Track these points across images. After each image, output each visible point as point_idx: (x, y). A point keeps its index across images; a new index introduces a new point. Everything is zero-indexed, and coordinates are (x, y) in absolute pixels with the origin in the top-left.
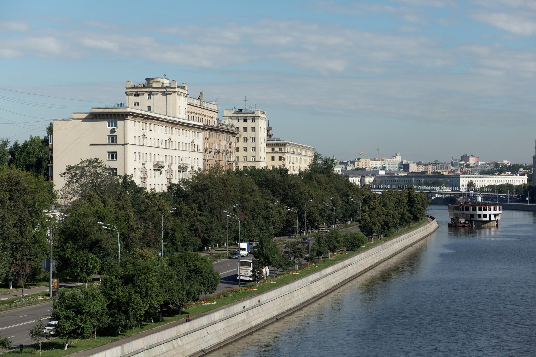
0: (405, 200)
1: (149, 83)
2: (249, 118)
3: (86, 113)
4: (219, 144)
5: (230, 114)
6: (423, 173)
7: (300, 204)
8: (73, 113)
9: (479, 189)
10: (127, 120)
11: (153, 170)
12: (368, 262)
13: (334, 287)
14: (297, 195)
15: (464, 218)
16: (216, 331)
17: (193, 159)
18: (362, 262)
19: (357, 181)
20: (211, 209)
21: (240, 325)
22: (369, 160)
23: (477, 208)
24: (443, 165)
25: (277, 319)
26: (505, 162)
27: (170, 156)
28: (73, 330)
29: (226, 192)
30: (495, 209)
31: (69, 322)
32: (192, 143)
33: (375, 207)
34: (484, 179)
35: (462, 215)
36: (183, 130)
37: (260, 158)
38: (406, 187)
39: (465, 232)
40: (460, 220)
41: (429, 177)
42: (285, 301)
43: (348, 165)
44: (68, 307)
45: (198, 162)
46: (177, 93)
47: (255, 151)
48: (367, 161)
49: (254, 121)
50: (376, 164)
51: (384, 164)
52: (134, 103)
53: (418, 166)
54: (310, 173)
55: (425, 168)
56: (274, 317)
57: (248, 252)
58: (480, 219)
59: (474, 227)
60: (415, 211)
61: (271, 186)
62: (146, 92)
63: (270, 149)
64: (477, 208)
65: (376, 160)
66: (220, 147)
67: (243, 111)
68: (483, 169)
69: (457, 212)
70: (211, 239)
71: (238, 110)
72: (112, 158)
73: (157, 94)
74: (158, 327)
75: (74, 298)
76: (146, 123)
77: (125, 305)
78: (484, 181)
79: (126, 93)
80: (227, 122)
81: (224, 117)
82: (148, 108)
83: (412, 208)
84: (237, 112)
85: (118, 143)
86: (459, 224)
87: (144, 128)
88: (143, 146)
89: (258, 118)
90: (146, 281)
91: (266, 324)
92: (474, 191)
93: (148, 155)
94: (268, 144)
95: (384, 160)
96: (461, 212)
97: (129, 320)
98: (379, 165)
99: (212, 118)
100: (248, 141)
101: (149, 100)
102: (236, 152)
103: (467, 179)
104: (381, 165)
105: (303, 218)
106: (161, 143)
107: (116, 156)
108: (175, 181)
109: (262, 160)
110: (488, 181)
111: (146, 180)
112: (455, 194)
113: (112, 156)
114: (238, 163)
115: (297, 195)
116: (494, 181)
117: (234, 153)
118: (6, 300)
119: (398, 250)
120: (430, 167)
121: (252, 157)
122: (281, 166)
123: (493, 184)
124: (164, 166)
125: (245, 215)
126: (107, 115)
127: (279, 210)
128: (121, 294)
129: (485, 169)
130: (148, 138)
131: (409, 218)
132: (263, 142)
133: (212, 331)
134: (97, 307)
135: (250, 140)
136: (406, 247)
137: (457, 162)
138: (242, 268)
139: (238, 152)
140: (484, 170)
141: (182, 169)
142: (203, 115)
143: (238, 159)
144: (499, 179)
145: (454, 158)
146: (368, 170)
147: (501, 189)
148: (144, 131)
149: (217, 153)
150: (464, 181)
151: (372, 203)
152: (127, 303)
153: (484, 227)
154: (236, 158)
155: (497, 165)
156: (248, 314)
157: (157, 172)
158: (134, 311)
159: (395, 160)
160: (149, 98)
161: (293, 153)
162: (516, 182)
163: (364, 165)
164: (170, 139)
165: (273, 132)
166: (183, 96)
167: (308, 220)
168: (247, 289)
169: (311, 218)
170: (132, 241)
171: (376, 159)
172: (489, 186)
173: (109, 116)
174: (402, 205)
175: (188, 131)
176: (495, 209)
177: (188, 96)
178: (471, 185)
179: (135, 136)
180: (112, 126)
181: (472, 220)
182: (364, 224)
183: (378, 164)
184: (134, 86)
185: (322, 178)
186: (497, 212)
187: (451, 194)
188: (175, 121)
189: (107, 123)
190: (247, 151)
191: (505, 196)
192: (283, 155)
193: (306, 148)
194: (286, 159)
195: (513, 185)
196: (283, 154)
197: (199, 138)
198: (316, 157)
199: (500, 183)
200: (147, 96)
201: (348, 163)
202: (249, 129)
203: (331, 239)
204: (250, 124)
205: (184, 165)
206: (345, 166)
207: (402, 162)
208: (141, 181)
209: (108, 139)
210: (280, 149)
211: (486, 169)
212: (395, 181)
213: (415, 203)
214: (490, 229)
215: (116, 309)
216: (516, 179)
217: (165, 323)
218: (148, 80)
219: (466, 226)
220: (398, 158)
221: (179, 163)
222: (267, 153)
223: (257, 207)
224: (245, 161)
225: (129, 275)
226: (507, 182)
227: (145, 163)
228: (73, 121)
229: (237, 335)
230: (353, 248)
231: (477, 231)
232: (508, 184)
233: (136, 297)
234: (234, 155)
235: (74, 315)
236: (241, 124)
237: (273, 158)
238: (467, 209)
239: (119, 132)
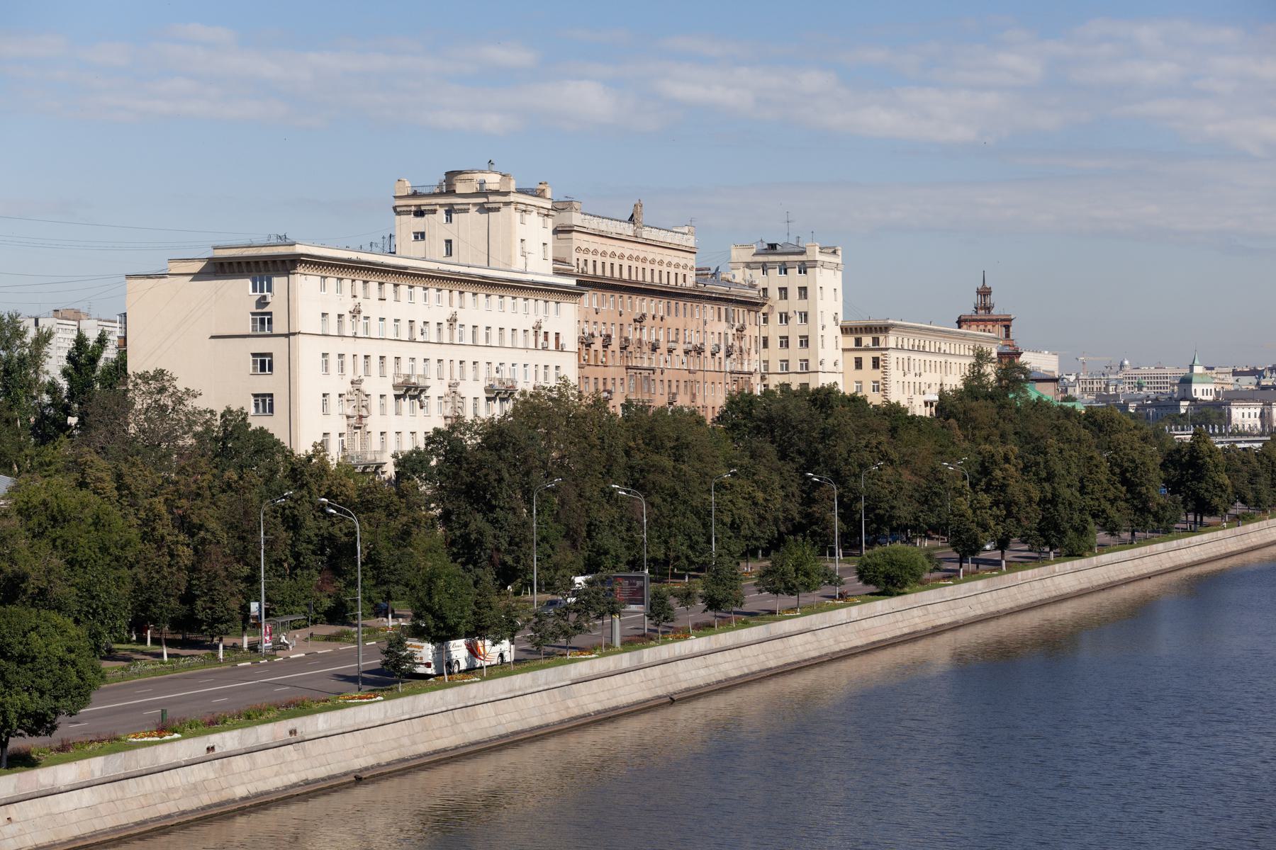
2: (792, 265)
3: (200, 260)
4: (701, 329)
5: (747, 256)
8: (171, 260)
10: (294, 274)
16: (51, 814)
19: (1252, 415)
43: (1264, 378)
46: (513, 207)
47: (807, 345)
52: (414, 233)
60: (1207, 490)
62: (441, 205)
63: (850, 342)
67: (778, 247)
71: (766, 247)
72: (263, 369)
73: (466, 211)
79: (395, 208)
81: (731, 265)
82: (447, 245)
83: (1199, 482)
85: (274, 332)
88: (354, 337)
89: (814, 264)
94: (846, 329)
100: (789, 322)
101: (449, 225)
105: (857, 512)
107: (271, 363)
111: (364, 422)
113: (263, 363)
114: (767, 376)
118: (84, 708)
121: (800, 360)
122: (878, 382)
124: (428, 387)
126: (248, 263)
138: (414, 644)
139: (766, 350)
143: (766, 368)
148: (357, 300)
154: (762, 365)
160: (449, 220)
165: (993, 299)
166: (534, 213)
169: (882, 512)
173: (253, 264)
180: (262, 291)
182: (958, 527)
189: (250, 284)
192: (883, 355)
196: (884, 352)
200: (445, 216)
202: (793, 293)
204: (794, 279)
206: (1256, 381)
208: (348, 425)
209: (253, 323)
210: (876, 341)
218: (451, 175)
222: (844, 350)
224: (784, 371)
228: (170, 279)
230: (890, 587)
236: (774, 280)
237: (859, 363)
239: (276, 304)
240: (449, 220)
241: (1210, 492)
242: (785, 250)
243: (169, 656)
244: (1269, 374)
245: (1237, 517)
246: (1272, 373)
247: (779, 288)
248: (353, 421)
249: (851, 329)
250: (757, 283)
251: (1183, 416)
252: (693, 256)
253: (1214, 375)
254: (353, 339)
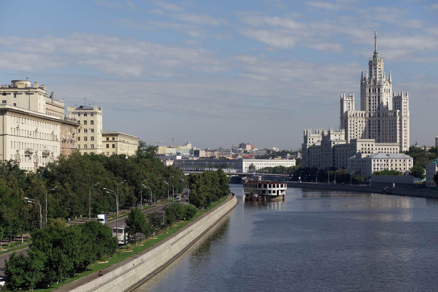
0: (218, 179)
1: (14, 85)
2: (89, 113)
5: (73, 110)
6: (212, 157)
7: (137, 183)
9: (258, 170)
11: (24, 156)
12: (202, 229)
13: (185, 248)
14: (134, 176)
15: (257, 193)
17: (53, 146)
18: (198, 229)
20: (73, 187)
21: (133, 279)
22: (166, 147)
23: (268, 185)
24: (226, 151)
25: (155, 274)
26: (275, 149)
27: (37, 145)
28: (22, 283)
29: (84, 174)
31: (20, 277)
32: (52, 133)
33: (199, 185)
34: (262, 162)
35: (255, 191)
36: (45, 123)
37: (98, 146)
38: (200, 169)
39: (259, 205)
40: (254, 195)
41: (217, 161)
42: (157, 260)
44: (18, 266)
45: (56, 149)
46: (38, 93)
47: (93, 140)
49: (93, 116)
50: (171, 150)
54: (137, 158)
55: (212, 154)
56: (152, 273)
57: (105, 221)
58: (270, 194)
59: (265, 201)
61: (113, 168)
62: (12, 92)
63: (105, 139)
64: (268, 185)
65: (171, 148)
66: (66, 137)
67: (83, 107)
68: (258, 154)
69: (252, 189)
70: (73, 212)
71: (79, 107)
73: (21, 94)
74: (75, 281)
75: (22, 258)
76: (19, 118)
77: (56, 264)
78: (262, 164)
80: (70, 116)
81: (67, 113)
84: (79, 109)
86: (254, 198)
87: (18, 122)
88: (17, 136)
89: (96, 113)
90: (71, 244)
91: (148, 278)
92: (256, 172)
93: (21, 143)
94: (104, 135)
95: (178, 147)
96: (255, 189)
97: (59, 275)
98: (173, 152)
99: (60, 113)
100: (87, 132)
101: (15, 98)
102: (78, 141)
103: (248, 162)
104: (176, 152)
105: (139, 194)
106: (30, 134)
108: (40, 165)
109: (99, 147)
110: (265, 164)
112: (240, 175)
114: (80, 150)
115: (134, 176)
117: (76, 142)
119: (218, 219)
120: (216, 153)
122: (114, 152)
123: (269, 166)
124: (33, 153)
125: (97, 192)
127: (123, 188)
128: (51, 255)
129: (260, 154)
130: (21, 130)
131: (221, 193)
132: (100, 133)
133: (116, 284)
134: (41, 265)
135: (89, 131)
136: (222, 217)
137: (236, 149)
140: (258, 155)
141: (45, 155)
142: (54, 111)
143: (79, 147)
144: (273, 163)
145: (234, 146)
146: (168, 155)
147: (275, 170)
148: (18, 124)
149: (64, 142)
150: (246, 164)
151: (198, 182)
152: (57, 262)
153: (273, 200)
154: (78, 146)
155: (268, 151)
156: (136, 270)
157: (27, 158)
158: (63, 268)
160: (15, 96)
161: (123, 142)
162: (287, 164)
163: (162, 151)
164: (36, 131)
167: (143, 196)
168: (125, 251)
170: (23, 213)
171: (171, 146)
172: (266, 168)
174: (215, 183)
175: (49, 124)
176: (282, 186)
177: (46, 95)
178: (252, 167)
179: (11, 128)
181: (263, 195)
182: (193, 199)
183: (174, 150)
184: (2, 87)
185: (148, 162)
186: (283, 188)
187: (236, 174)
188: (41, 116)
190: (93, 140)
191: (279, 176)
193: (132, 138)
194: (118, 147)
195: (285, 167)
196: (116, 143)
197: (57, 129)
198: (141, 144)
199: (275, 166)
200: (13, 95)
202: (89, 123)
203: (174, 210)
204: (89, 118)
205: (46, 152)
207: (192, 149)
210: (113, 139)
211: (261, 154)
213: (223, 181)
214: (278, 202)
215: (48, 267)
216: (287, 163)
217: (80, 278)
218: (14, 82)
219: (259, 200)
220: (189, 146)
221: (43, 150)
223: (107, 185)
224: (85, 148)
225: (57, 240)
226: (280, 165)
227: (19, 150)
229: (132, 287)
231: (268, 203)
232: (281, 166)
233: (64, 256)
234: (76, 143)
235: (23, 271)
236: (82, 118)
238: (260, 186)
240: (15, 96)
241: (224, 188)
242: (85, 108)
243: (23, 240)
247: (84, 121)
248: (36, 164)
249: (105, 135)
250: (76, 119)
252: (63, 110)
254: (17, 137)
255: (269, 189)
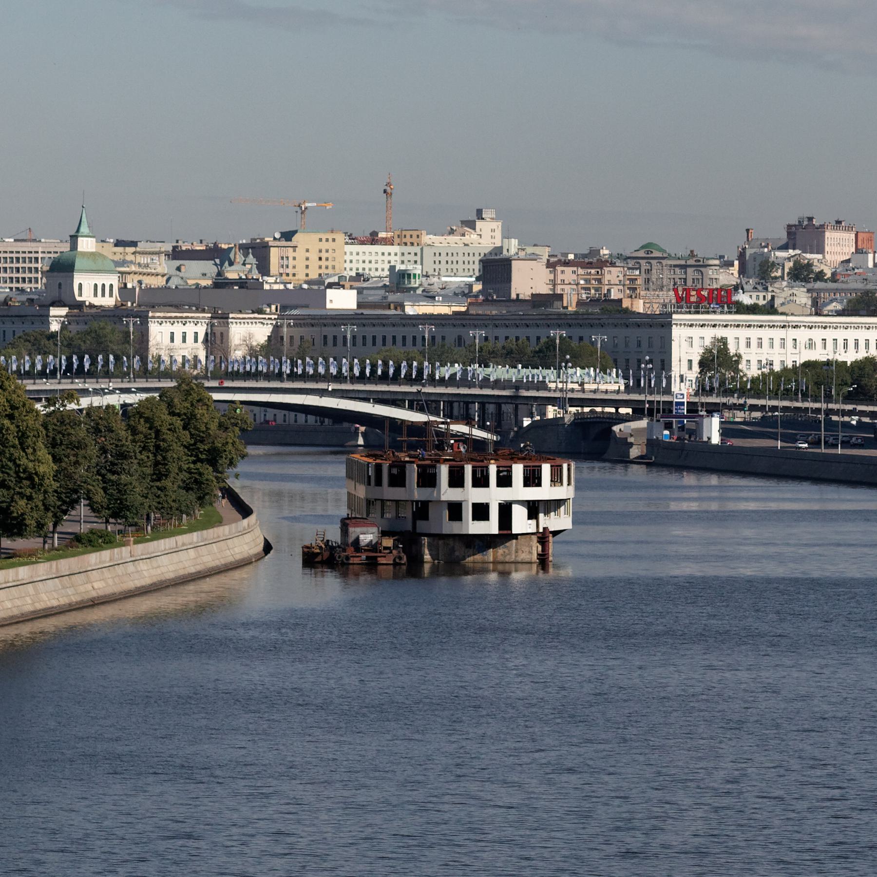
19: (190, 338)
22: (341, 238)
23: (444, 471)
30: (532, 479)
34: (792, 333)
43: (231, 264)
48: (330, 245)
50: (373, 258)
51: (412, 258)
53: (554, 272)
55: (587, 281)
58: (454, 528)
59: (427, 567)
64: (444, 471)
78: (789, 343)
86: (350, 551)
95: (414, 240)
116: (841, 343)
145: (753, 235)
146: (276, 287)
159: (467, 239)
163: (314, 263)
171: (382, 235)
176: (532, 479)
181: (418, 530)
186: (545, 492)
187: (617, 404)
199: (861, 355)
201: (232, 256)
206: (215, 270)
212: (340, 341)
219: (382, 560)
244: (240, 258)
245: (78, 539)
246: (246, 255)
251: (53, 335)
253: (130, 258)
255: (448, 493)
